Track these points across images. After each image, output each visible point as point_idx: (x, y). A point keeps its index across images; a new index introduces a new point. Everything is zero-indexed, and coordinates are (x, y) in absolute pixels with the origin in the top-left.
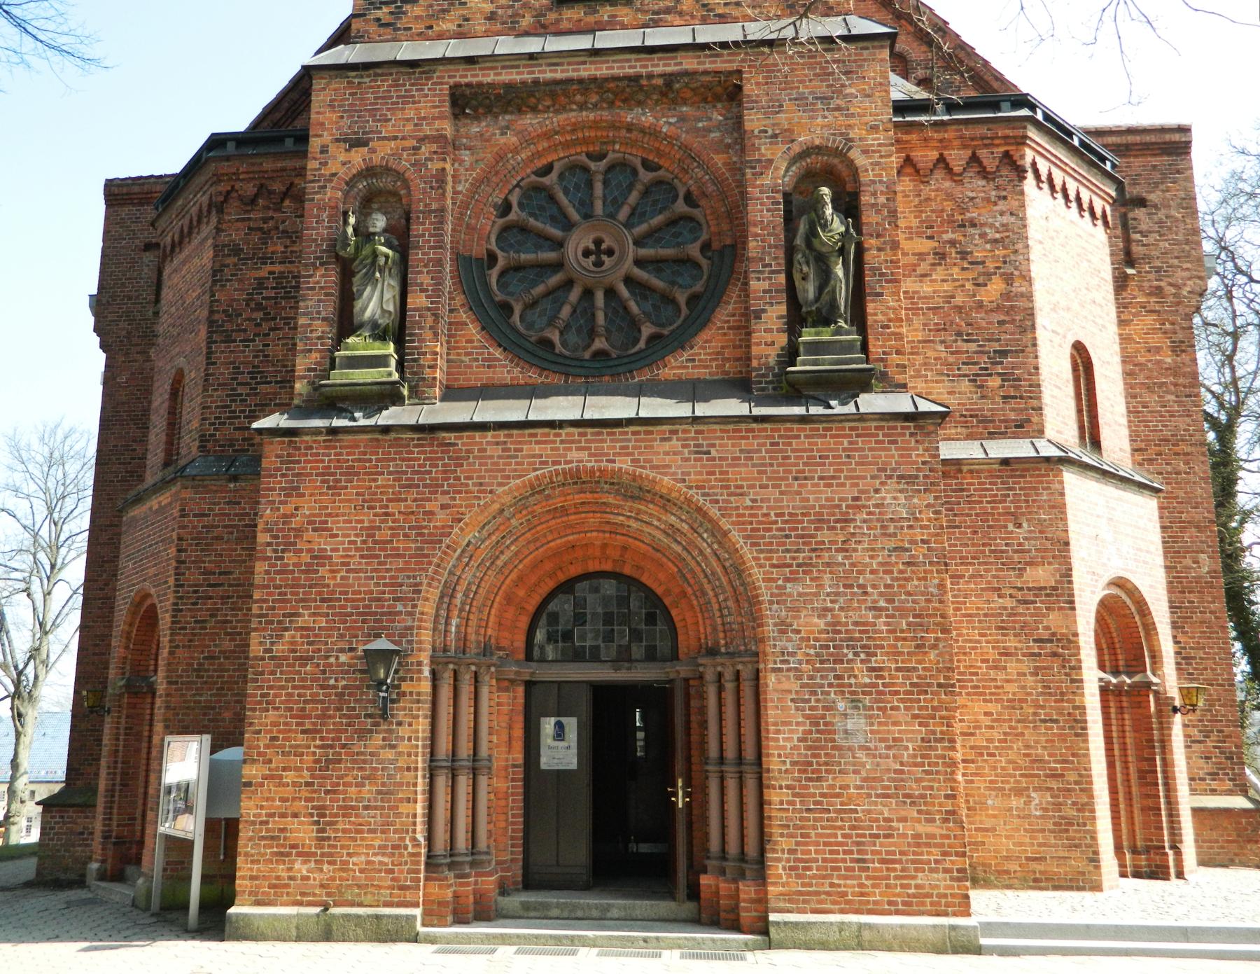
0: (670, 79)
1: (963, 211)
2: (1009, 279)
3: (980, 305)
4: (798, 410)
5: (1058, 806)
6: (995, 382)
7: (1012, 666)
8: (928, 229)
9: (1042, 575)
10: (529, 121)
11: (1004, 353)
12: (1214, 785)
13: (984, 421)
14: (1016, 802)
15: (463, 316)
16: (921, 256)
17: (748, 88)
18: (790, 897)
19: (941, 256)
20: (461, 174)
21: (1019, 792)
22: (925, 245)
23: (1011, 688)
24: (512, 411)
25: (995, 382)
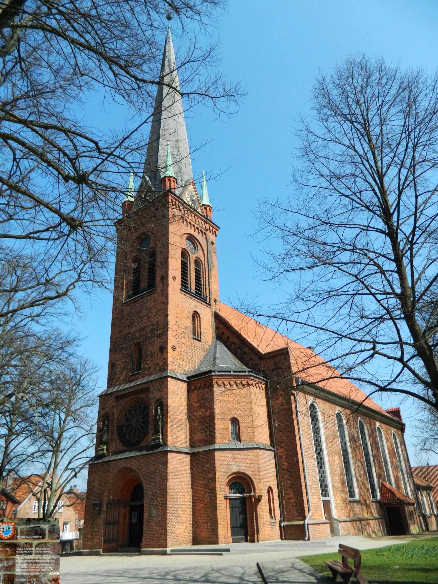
0: (141, 389)
1: (204, 396)
2: (211, 410)
3: (206, 416)
4: (151, 452)
5: (212, 526)
6: (208, 433)
7: (206, 495)
8: (199, 402)
9: (211, 475)
10: (127, 400)
11: (209, 426)
12: (299, 518)
13: (207, 441)
14: (206, 525)
15: (117, 438)
16: (197, 407)
17: (150, 390)
18: (145, 545)
19: (201, 406)
20: (116, 412)
21: (206, 523)
22: (198, 405)
23: (206, 500)
24: (125, 455)
25: (208, 433)
